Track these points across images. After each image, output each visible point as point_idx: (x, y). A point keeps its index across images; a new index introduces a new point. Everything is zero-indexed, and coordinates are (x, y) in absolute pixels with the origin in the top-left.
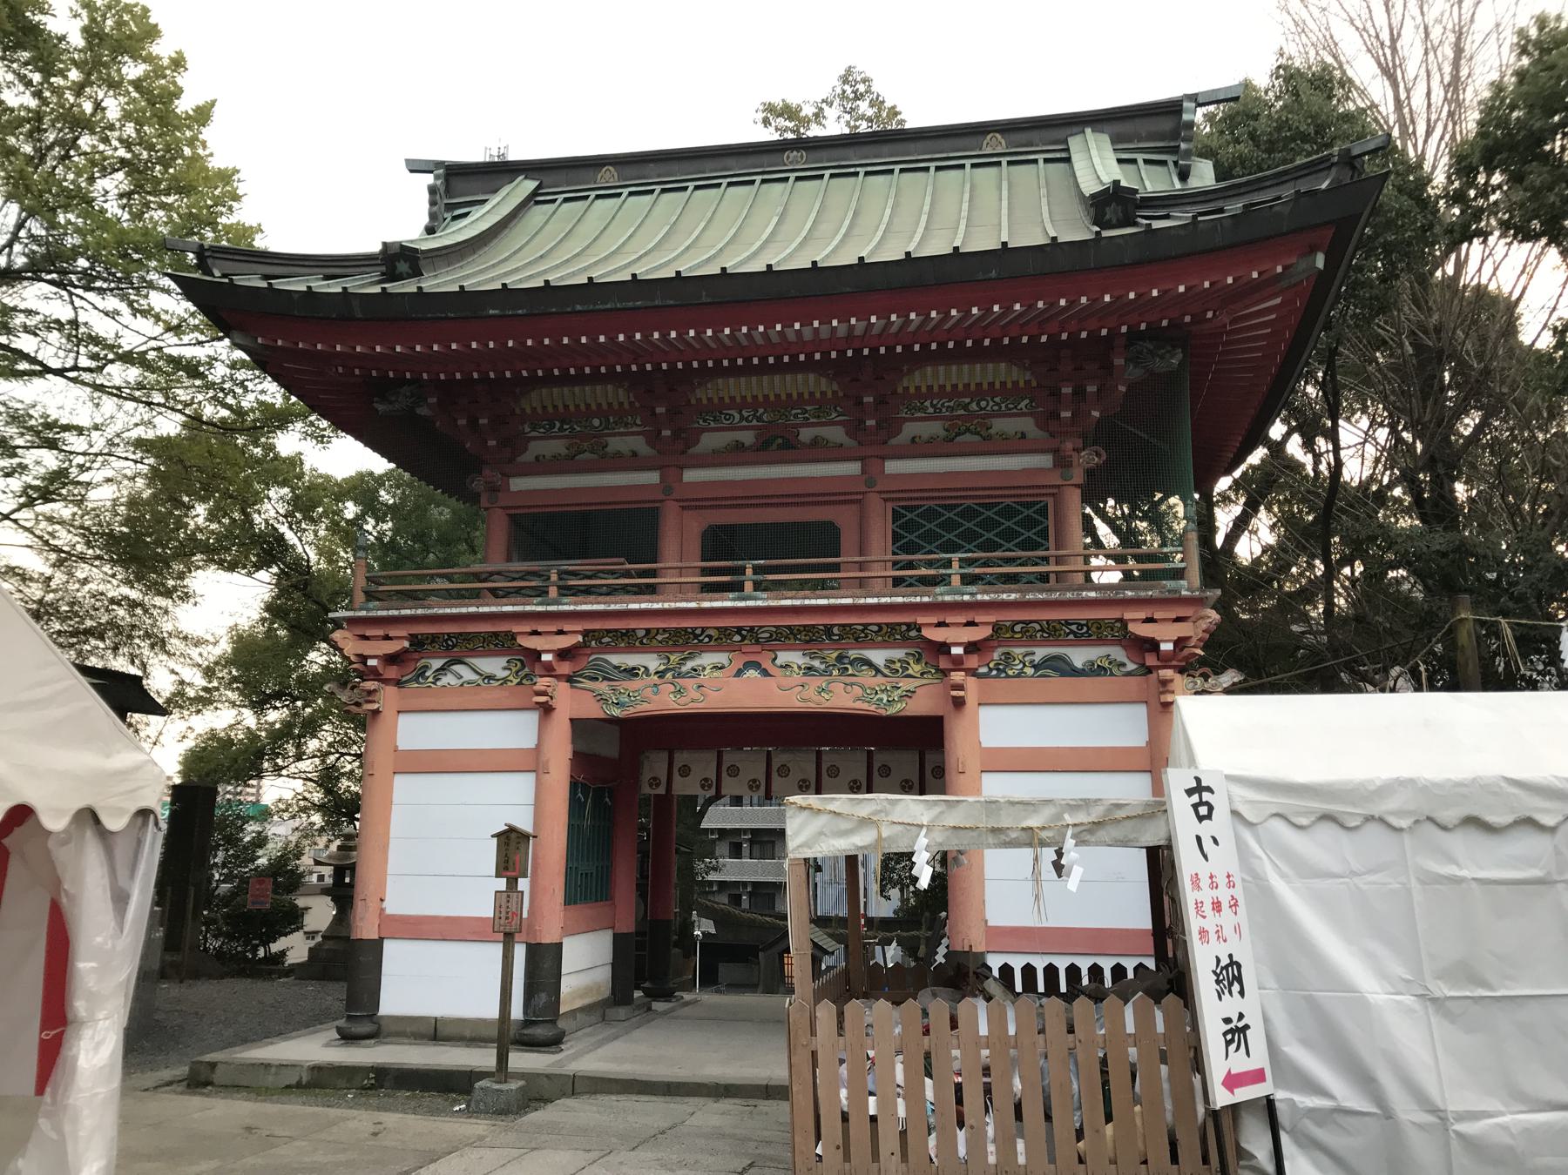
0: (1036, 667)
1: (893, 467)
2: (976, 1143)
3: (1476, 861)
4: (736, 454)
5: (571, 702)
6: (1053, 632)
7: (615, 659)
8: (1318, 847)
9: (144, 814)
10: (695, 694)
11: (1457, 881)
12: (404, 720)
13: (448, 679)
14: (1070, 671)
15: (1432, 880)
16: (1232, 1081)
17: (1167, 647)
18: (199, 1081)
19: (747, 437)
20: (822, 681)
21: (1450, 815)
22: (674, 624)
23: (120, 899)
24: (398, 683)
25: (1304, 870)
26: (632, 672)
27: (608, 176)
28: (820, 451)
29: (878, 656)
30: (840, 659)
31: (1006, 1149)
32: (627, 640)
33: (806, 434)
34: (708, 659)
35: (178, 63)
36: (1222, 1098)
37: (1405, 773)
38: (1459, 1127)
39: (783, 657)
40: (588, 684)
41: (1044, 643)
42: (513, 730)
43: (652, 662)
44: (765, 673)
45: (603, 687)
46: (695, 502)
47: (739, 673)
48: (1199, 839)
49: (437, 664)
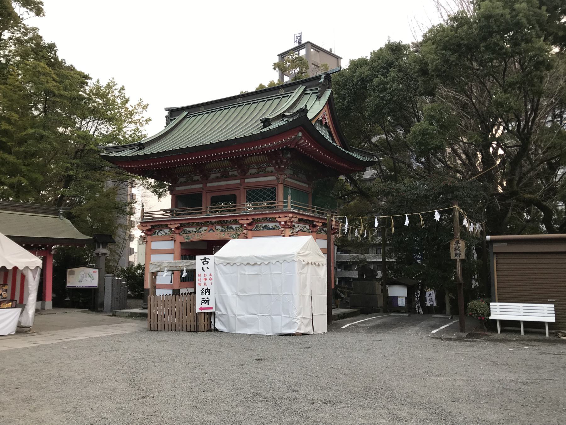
0: (262, 228)
1: (247, 181)
2: (170, 319)
3: (249, 271)
4: (217, 179)
5: (180, 238)
6: (265, 220)
7: (188, 229)
8: (225, 269)
9: (38, 267)
10: (201, 236)
11: (245, 274)
12: (152, 243)
13: (160, 234)
14: (268, 229)
15: (241, 274)
16: (201, 309)
17: (283, 223)
18: (114, 315)
19: (219, 175)
20: (223, 233)
21: (245, 263)
22: (197, 221)
23: (34, 278)
24: (151, 235)
25: (224, 273)
26: (190, 232)
27: (202, 109)
28: (233, 177)
29: (234, 227)
30: (227, 227)
31: (174, 320)
32: (189, 225)
33: (230, 173)
34: (204, 228)
35: (123, 89)
36: (198, 311)
37: (240, 255)
38: (239, 317)
39: (218, 227)
40: (183, 235)
41: (264, 222)
42: (168, 245)
43: (194, 229)
44: (214, 231)
45: (185, 235)
46: (210, 191)
47: (209, 231)
48: (203, 268)
49: (157, 231)
